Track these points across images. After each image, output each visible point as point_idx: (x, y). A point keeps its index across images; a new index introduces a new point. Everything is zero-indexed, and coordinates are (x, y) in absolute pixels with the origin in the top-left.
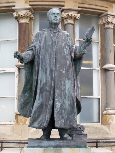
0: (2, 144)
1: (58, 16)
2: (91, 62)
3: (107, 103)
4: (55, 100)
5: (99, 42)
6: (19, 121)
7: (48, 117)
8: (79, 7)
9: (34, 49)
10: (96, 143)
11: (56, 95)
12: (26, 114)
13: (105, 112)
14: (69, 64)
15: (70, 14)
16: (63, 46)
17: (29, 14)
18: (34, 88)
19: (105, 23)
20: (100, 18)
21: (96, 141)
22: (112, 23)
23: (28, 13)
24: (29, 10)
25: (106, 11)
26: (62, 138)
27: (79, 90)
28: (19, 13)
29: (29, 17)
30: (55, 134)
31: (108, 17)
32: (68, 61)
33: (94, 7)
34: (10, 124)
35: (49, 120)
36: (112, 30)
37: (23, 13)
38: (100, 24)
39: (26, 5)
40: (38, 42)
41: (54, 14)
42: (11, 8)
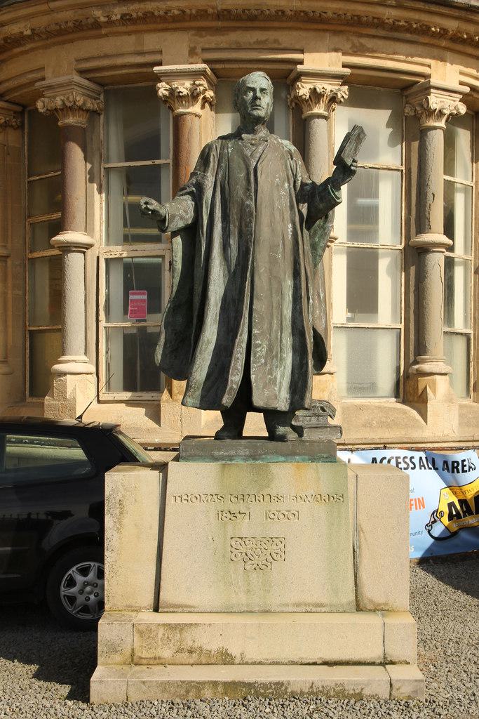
1: (264, 97)
2: (130, 236)
4: (253, 332)
6: (176, 392)
8: (344, 66)
15: (321, 85)
20: (407, 97)
25: (427, 76)
26: (273, 437)
28: (175, 85)
29: (202, 96)
30: (254, 424)
34: (153, 399)
37: (184, 84)
42: (149, 70)
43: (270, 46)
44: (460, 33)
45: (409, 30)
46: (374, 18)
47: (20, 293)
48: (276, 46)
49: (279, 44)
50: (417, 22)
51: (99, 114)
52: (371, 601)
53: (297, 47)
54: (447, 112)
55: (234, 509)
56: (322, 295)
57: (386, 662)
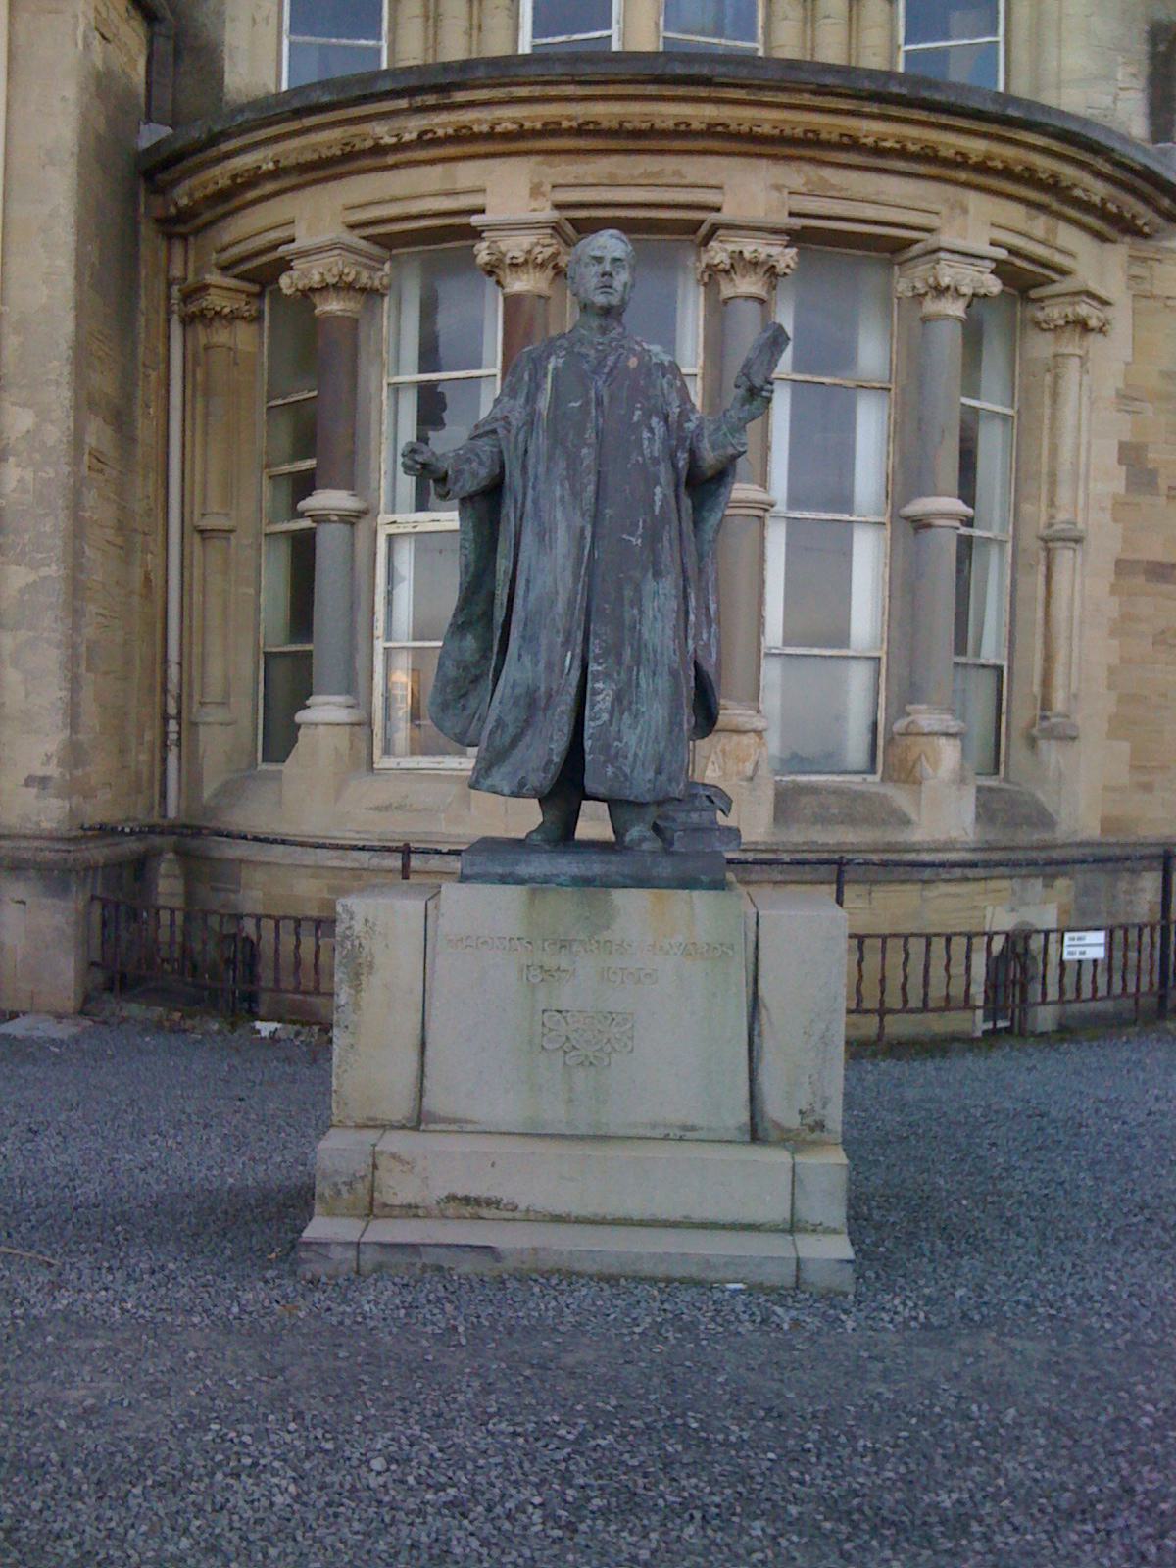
0: (409, 858)
3: (912, 684)
4: (590, 669)
5: (892, 386)
7: (559, 744)
8: (791, 214)
9: (501, 432)
10: (835, 867)
11: (595, 648)
12: (465, 733)
13: (900, 725)
14: (662, 506)
15: (750, 246)
16: (635, 418)
17: (549, 251)
18: (499, 616)
19: (922, 291)
21: (836, 856)
22: (956, 290)
23: (544, 246)
24: (549, 231)
27: (709, 627)
30: (594, 822)
31: (938, 261)
32: (658, 490)
33: (870, 212)
35: (556, 759)
36: (959, 325)
38: (899, 298)
39: (534, 204)
40: (522, 400)
41: (599, 260)
43: (665, 181)
44: (991, 158)
45: (902, 153)
46: (842, 135)
47: (251, 591)
48: (675, 180)
49: (683, 177)
50: (915, 141)
51: (383, 296)
52: (777, 1125)
53: (713, 182)
54: (966, 290)
55: (550, 962)
56: (713, 607)
57: (793, 1227)
